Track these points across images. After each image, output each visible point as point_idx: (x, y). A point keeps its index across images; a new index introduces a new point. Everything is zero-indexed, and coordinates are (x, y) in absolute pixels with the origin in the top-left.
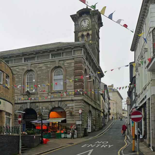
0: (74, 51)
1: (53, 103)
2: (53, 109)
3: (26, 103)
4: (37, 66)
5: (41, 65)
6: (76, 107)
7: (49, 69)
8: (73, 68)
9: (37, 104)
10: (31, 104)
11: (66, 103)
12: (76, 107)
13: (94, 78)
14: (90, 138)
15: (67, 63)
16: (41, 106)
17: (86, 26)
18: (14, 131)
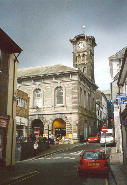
0: (71, 75)
1: (56, 115)
2: (57, 120)
3: (35, 115)
4: (44, 86)
5: (46, 85)
6: (74, 118)
7: (53, 89)
8: (71, 88)
9: (44, 116)
10: (39, 116)
11: (66, 115)
12: (74, 118)
13: (89, 92)
14: (85, 143)
15: (67, 84)
16: (47, 118)
17: (82, 48)
18: (50, 134)
